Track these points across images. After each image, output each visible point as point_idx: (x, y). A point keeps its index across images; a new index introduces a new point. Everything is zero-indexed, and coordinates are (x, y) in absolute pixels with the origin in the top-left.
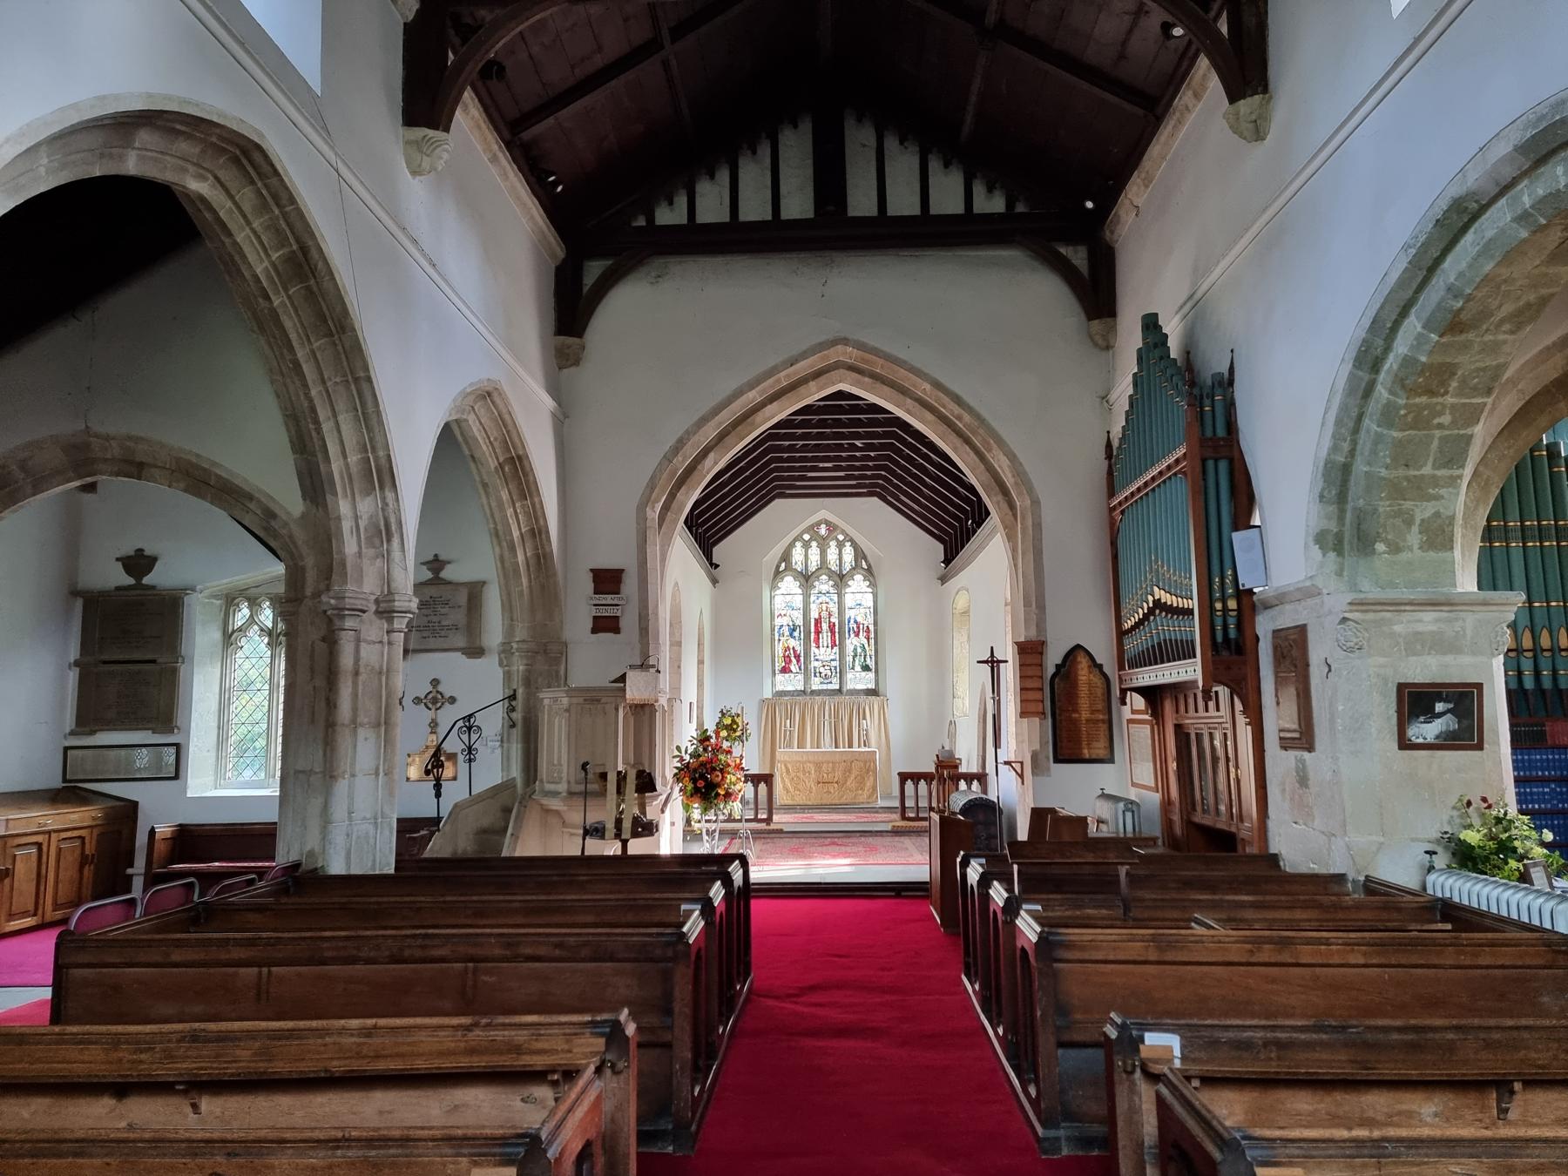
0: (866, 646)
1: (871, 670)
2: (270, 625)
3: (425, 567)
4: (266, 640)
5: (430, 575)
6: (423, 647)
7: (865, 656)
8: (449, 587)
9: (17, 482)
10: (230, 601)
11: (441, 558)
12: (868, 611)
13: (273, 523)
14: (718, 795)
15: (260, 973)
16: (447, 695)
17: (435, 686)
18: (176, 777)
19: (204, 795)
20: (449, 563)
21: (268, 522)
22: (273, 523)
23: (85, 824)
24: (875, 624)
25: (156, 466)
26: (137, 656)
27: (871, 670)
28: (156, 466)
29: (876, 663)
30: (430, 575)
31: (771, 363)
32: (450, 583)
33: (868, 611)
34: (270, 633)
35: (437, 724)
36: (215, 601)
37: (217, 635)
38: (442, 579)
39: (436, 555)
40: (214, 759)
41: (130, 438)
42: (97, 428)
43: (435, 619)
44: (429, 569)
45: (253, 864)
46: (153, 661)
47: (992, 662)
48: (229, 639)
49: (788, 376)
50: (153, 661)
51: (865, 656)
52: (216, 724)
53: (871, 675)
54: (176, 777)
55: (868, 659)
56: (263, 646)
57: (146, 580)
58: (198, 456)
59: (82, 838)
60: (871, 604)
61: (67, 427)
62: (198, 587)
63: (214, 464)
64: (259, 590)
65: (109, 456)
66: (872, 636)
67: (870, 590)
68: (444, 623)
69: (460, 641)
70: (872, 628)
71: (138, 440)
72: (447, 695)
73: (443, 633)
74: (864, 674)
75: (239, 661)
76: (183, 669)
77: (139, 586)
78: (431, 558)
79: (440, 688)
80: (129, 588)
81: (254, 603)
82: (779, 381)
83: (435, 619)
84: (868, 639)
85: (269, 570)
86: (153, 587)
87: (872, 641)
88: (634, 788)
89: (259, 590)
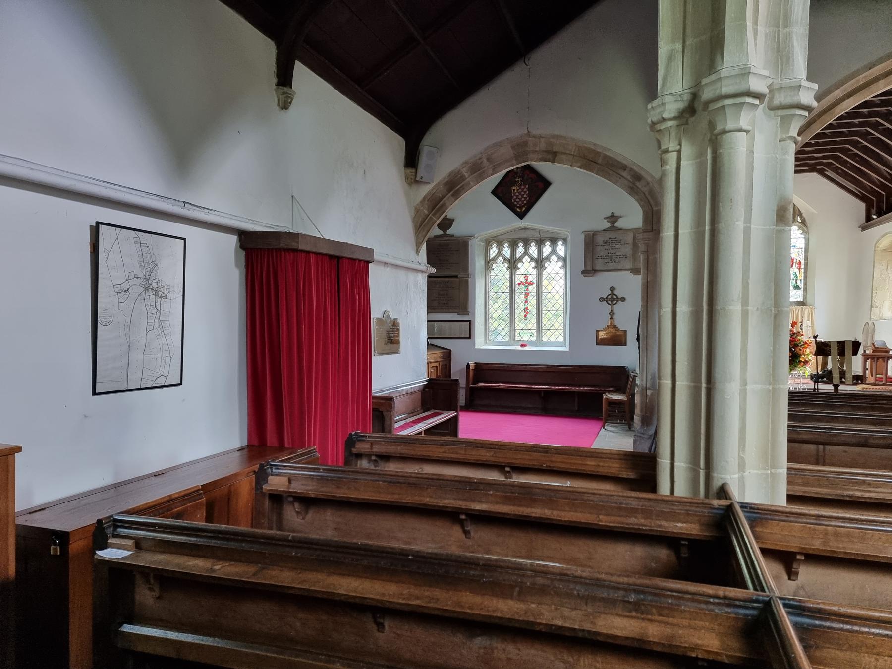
0: (798, 273)
1: (800, 289)
2: (509, 257)
3: (606, 220)
4: (507, 265)
5: (608, 225)
6: (605, 268)
7: (797, 280)
8: (621, 232)
9: (484, 168)
10: (488, 244)
11: (616, 214)
12: (800, 250)
13: (638, 184)
14: (800, 362)
15: (818, 450)
16: (620, 297)
17: (612, 291)
18: (470, 338)
19: (482, 348)
20: (621, 217)
21: (634, 184)
22: (638, 184)
23: (436, 360)
24: (806, 258)
25: (565, 153)
26: (445, 274)
27: (800, 289)
28: (565, 153)
29: (805, 285)
30: (608, 225)
31: (854, 69)
32: (621, 229)
33: (800, 250)
34: (564, 260)
35: (614, 313)
36: (481, 243)
37: (483, 262)
38: (617, 228)
39: (613, 213)
40: (483, 330)
41: (554, 137)
42: (534, 132)
43: (612, 251)
44: (608, 221)
45: (533, 386)
46: (456, 276)
47: (612, 300)
48: (488, 264)
49: (865, 77)
50: (456, 276)
51: (797, 280)
52: (484, 311)
53: (801, 292)
54: (470, 338)
55: (799, 283)
56: (504, 268)
57: (449, 232)
58: (595, 144)
59: (436, 367)
60: (803, 246)
61: (517, 132)
62: (476, 236)
63: (605, 149)
64: (503, 237)
65: (537, 149)
66: (803, 266)
67: (803, 236)
68: (617, 254)
69: (628, 264)
70: (803, 262)
71: (558, 137)
72: (620, 297)
73: (617, 260)
74: (795, 291)
75: (492, 277)
76: (470, 280)
77: (445, 235)
78: (609, 214)
79: (616, 292)
80: (440, 236)
81: (500, 245)
82: (859, 81)
83: (612, 251)
84: (799, 269)
85: (513, 225)
86: (453, 236)
87: (802, 271)
88: (837, 353)
89: (503, 237)
